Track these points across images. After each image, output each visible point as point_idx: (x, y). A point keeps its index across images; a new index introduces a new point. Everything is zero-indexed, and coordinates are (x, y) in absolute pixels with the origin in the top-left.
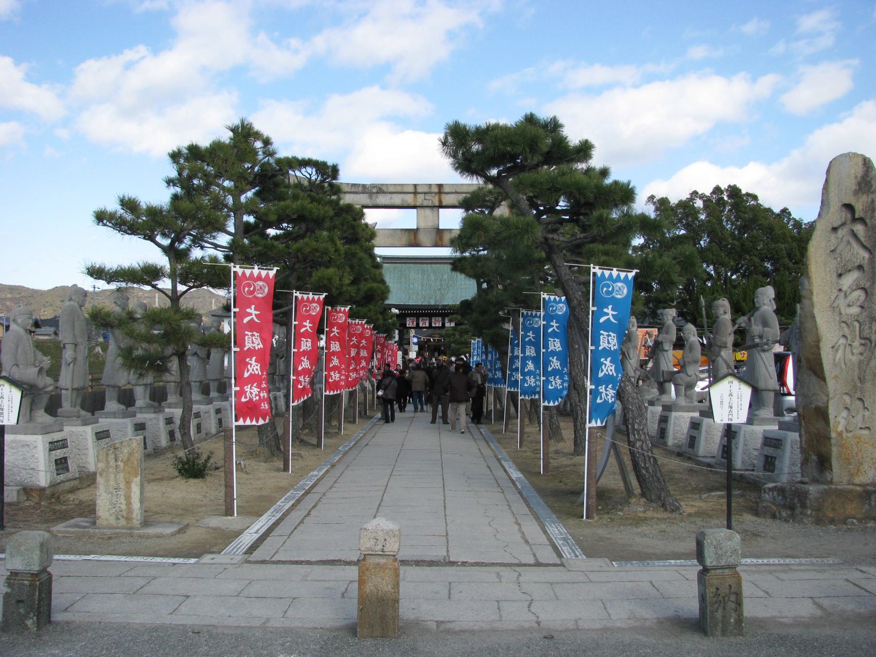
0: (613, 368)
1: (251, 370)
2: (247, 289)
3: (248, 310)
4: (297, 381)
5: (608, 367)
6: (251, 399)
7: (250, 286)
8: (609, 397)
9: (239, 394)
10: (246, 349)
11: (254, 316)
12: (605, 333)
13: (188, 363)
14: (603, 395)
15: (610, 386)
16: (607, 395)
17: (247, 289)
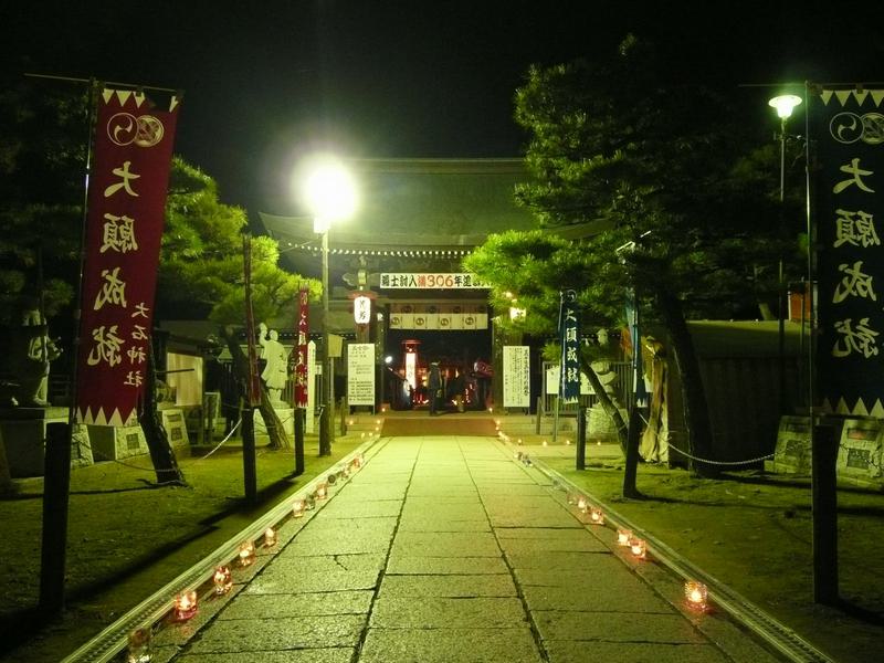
1: (107, 293)
6: (104, 363)
8: (865, 345)
14: (100, 347)
15: (113, 329)
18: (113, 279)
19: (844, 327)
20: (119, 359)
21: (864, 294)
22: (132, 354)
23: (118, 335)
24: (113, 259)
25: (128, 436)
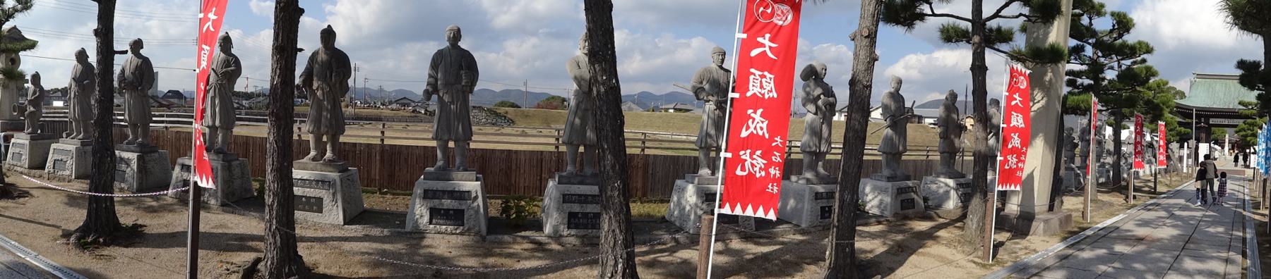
0: (764, 126)
1: (752, 127)
2: (769, 11)
3: (760, 40)
4: (1006, 161)
5: (758, 124)
6: (751, 175)
7: (766, 7)
8: (757, 169)
9: (1003, 163)
10: (749, 94)
11: (767, 49)
12: (758, 73)
13: (575, 86)
14: (747, 164)
15: (759, 152)
16: (753, 165)
17: (769, 11)
18: (757, 117)
19: (745, 155)
20: (763, 173)
21: (760, 133)
22: (772, 171)
23: (762, 157)
24: (757, 102)
25: (321, 212)
